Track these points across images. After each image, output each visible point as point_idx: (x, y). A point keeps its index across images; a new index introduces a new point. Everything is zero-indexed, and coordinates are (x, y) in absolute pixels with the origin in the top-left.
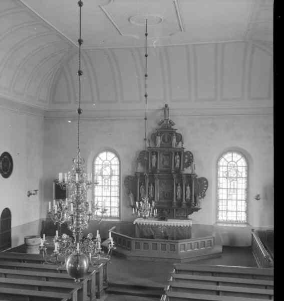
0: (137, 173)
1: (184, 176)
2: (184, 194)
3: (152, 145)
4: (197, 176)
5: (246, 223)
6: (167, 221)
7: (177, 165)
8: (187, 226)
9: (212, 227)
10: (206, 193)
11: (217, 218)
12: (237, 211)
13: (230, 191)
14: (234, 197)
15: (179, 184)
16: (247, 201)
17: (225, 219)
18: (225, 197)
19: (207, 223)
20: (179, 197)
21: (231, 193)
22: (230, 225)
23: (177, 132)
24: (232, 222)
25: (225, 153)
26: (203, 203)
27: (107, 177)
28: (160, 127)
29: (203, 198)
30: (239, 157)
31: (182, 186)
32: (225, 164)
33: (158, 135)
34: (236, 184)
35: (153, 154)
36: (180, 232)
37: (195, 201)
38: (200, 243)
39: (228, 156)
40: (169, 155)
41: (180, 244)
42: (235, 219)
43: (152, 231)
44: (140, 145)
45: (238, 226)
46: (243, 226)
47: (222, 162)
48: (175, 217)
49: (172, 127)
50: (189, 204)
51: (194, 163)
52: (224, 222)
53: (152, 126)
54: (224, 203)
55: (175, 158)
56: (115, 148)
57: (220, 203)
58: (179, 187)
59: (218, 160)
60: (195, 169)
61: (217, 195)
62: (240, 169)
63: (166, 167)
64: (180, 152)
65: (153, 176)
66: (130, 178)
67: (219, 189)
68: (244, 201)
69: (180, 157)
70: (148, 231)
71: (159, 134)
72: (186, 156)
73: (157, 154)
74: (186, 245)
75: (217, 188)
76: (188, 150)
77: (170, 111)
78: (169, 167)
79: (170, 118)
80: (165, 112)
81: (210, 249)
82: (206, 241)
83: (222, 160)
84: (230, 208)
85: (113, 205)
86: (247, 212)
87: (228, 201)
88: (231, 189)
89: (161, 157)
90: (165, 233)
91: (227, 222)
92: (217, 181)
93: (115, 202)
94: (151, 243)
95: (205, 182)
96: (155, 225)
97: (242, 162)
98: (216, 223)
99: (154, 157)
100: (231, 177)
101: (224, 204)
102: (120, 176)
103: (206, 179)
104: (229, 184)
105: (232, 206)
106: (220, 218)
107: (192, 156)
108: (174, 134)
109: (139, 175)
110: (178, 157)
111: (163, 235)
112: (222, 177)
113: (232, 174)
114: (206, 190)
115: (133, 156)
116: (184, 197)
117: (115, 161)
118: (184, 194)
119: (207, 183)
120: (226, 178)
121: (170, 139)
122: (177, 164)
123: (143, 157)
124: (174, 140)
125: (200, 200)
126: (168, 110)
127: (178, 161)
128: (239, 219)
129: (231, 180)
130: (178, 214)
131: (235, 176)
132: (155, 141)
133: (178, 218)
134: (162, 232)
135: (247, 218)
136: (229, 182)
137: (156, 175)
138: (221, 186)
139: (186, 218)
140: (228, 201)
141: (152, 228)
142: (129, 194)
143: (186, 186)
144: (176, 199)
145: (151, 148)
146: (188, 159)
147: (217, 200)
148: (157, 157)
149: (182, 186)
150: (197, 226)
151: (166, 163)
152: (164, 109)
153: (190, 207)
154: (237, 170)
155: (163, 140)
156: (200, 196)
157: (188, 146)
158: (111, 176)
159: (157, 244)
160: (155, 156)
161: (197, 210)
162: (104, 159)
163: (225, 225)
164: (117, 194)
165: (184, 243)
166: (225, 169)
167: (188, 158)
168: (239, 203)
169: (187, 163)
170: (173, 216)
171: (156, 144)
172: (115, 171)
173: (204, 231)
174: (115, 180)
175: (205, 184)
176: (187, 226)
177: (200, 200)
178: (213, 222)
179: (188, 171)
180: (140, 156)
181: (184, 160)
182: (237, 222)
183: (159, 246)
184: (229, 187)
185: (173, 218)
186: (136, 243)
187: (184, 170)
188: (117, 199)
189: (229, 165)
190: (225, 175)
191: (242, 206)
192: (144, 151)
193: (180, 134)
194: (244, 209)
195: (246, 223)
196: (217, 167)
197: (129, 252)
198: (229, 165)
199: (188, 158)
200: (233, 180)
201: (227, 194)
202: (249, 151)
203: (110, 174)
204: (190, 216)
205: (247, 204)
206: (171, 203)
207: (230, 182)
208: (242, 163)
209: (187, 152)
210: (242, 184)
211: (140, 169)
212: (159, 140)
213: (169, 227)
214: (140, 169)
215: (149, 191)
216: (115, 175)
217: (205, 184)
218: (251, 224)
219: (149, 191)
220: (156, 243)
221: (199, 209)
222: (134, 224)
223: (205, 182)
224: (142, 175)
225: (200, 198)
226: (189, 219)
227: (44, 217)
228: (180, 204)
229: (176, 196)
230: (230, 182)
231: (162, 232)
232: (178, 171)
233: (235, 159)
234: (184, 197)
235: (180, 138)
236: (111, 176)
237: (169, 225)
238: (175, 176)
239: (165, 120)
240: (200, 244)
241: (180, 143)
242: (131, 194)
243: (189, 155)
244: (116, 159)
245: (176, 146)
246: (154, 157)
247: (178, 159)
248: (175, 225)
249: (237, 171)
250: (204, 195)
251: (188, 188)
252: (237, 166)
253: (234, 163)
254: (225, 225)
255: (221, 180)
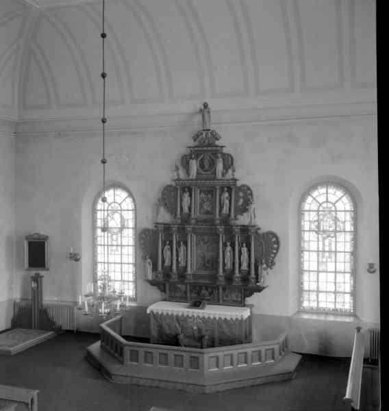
0: (157, 223)
1: (237, 230)
2: (237, 260)
3: (182, 175)
4: (259, 229)
5: (350, 315)
6: (203, 309)
7: (225, 210)
8: (237, 319)
9: (289, 320)
10: (276, 260)
11: (300, 302)
12: (335, 293)
13: (323, 257)
14: (331, 267)
15: (228, 244)
16: (354, 273)
17: (314, 305)
18: (314, 267)
19: (278, 314)
20: (229, 266)
21: (325, 260)
22: (322, 318)
23: (225, 150)
24: (326, 312)
25: (314, 187)
26: (269, 278)
27: (115, 231)
28: (197, 143)
29: (271, 268)
30: (339, 193)
31: (233, 246)
32: (124, 206)
33: (191, 158)
34: (333, 244)
35: (184, 191)
36: (226, 330)
37: (257, 274)
38: (276, 348)
39: (320, 194)
40: (211, 191)
41: (206, 356)
42: (331, 306)
43: (177, 325)
44: (165, 176)
45: (339, 319)
46: (348, 320)
47: (309, 204)
48: (221, 302)
49: (217, 143)
50: (245, 279)
51: (253, 206)
52: (311, 311)
53: (184, 142)
54: (313, 276)
55: (222, 198)
56: (126, 182)
57: (306, 277)
58: (229, 248)
59: (302, 199)
60: (255, 217)
61: (300, 263)
62: (341, 216)
63: (207, 213)
64: (230, 188)
65: (184, 229)
66: (147, 233)
67: (302, 252)
68: (349, 275)
69: (230, 195)
70: (172, 326)
71: (193, 156)
72: (241, 194)
73: (190, 190)
74: (234, 355)
75: (300, 251)
76: (244, 183)
77: (211, 113)
78: (211, 213)
79: (212, 127)
80: (203, 116)
81: (272, 365)
82: (263, 349)
83: (310, 199)
84: (322, 287)
85: (125, 277)
86: (354, 294)
87: (320, 274)
88: (324, 251)
89: (198, 196)
90: (199, 330)
91: (319, 311)
92: (300, 239)
93: (129, 272)
94: (171, 351)
95: (274, 239)
96: (183, 315)
97: (345, 204)
98: (299, 312)
99: (186, 195)
100: (324, 231)
101: (311, 279)
102: (135, 228)
103: (274, 235)
104: (321, 244)
105: (326, 282)
106: (306, 304)
107: (251, 194)
108: (219, 155)
109: (161, 227)
110: (226, 195)
111: (196, 334)
112: (309, 231)
113: (327, 224)
114: (275, 254)
115: (154, 194)
116: (237, 266)
117: (128, 204)
118: (237, 260)
119: (278, 242)
120: (316, 232)
121: (213, 164)
122: (225, 208)
123: (170, 196)
124: (220, 166)
125: (264, 273)
126: (209, 112)
127: (227, 202)
128: (339, 306)
129: (325, 236)
130: (227, 296)
131: (331, 229)
132: (186, 166)
133: (226, 303)
134: (195, 328)
135: (355, 306)
136: (321, 239)
137: (189, 228)
138: (306, 246)
139: (241, 304)
140: (320, 274)
141: (177, 320)
142: (144, 258)
143: (241, 246)
144: (240, 271)
145: (181, 180)
146: (244, 198)
147: (300, 272)
148: (190, 196)
149: (233, 246)
150: (264, 317)
151: (206, 207)
152: (201, 110)
153: (247, 286)
154: (336, 217)
155: (202, 166)
156: (265, 266)
157: (242, 176)
158: (122, 228)
159: (167, 354)
160: (188, 194)
161: (260, 290)
162: (322, 199)
163: (315, 317)
164: (131, 260)
165: (232, 352)
166: (313, 216)
167: (243, 197)
168: (340, 278)
169: (242, 205)
170: (219, 300)
171: (188, 173)
172: (128, 220)
173: (274, 327)
174: (129, 237)
175: (275, 243)
176: (237, 319)
177: (264, 273)
178: (290, 311)
179: (243, 220)
180: (163, 194)
181: (237, 201)
182: (335, 312)
183: (186, 357)
184: (321, 249)
185: (217, 302)
186: (131, 351)
187: (236, 219)
188: (131, 269)
189: (321, 209)
190: (313, 227)
191: (346, 283)
192: (171, 186)
193: (229, 155)
194: (348, 288)
195: (350, 315)
196: (300, 213)
197: (118, 366)
198: (321, 209)
199: (243, 197)
200: (329, 236)
201: (318, 262)
202: (354, 181)
203: (119, 226)
204: (249, 300)
205: (355, 282)
206: (215, 278)
207: (324, 239)
208: (128, 204)
209: (244, 186)
210: (344, 243)
211: (165, 217)
212: (194, 166)
213: (205, 321)
214: (165, 217)
215: (177, 256)
216: (128, 228)
217: (275, 243)
218: (359, 315)
219: (177, 256)
220: (165, 352)
221: (264, 288)
222: (148, 312)
223: (274, 239)
224: (167, 228)
225: (265, 269)
226: (244, 306)
227: (17, 296)
228: (229, 278)
229: (224, 265)
230: (324, 239)
231: (195, 328)
232: (226, 221)
233: (332, 198)
234: (237, 266)
235: (229, 163)
236: (122, 228)
237: (206, 317)
238: (221, 229)
239: (204, 130)
240: (249, 356)
241: (230, 171)
242: (149, 260)
243: (245, 193)
244: (129, 200)
245: (223, 175)
246: (186, 197)
247: (227, 198)
248: (212, 317)
249: (336, 219)
250: (273, 264)
251: (244, 250)
252: (336, 211)
253: (330, 205)
254: (315, 317)
255: (306, 236)
